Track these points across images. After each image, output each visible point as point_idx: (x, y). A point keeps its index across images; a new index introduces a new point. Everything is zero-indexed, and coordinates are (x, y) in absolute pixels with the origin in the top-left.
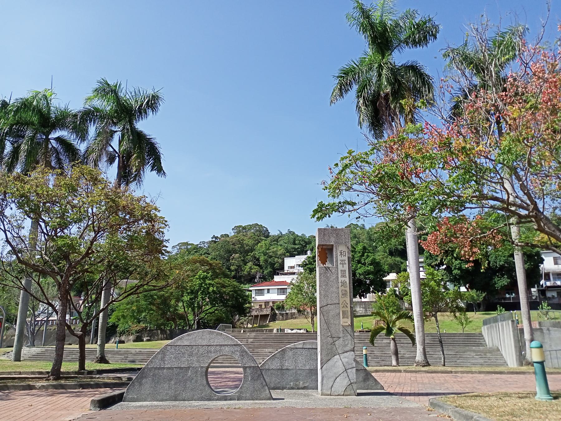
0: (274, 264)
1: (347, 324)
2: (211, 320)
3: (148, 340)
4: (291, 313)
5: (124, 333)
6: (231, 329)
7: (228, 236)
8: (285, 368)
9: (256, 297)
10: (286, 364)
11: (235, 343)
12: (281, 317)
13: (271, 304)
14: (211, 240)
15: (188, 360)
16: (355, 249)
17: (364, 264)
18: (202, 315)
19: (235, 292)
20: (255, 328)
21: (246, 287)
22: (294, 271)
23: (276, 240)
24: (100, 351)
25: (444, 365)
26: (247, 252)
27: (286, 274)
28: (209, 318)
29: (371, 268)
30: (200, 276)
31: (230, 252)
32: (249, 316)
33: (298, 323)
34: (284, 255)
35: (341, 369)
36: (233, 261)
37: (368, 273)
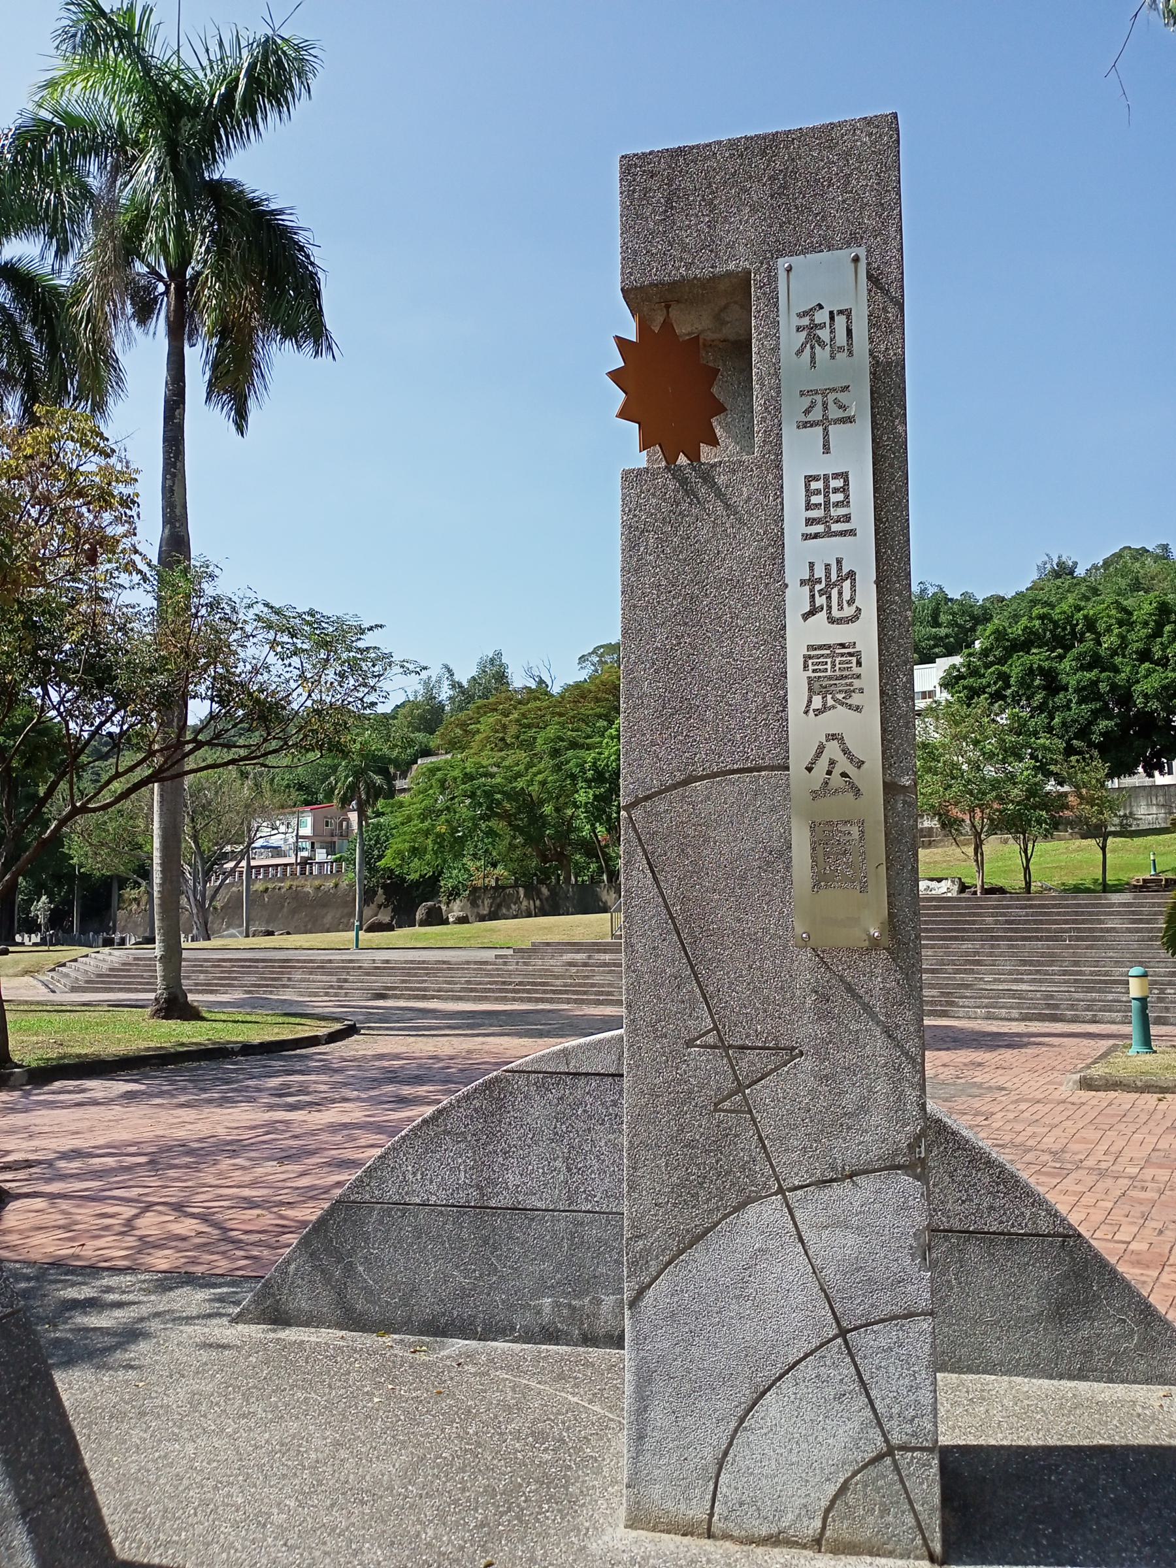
5: (458, 894)
8: (504, 1200)
16: (1130, 614)
24: (164, 978)
33: (938, 858)
35: (797, 1317)
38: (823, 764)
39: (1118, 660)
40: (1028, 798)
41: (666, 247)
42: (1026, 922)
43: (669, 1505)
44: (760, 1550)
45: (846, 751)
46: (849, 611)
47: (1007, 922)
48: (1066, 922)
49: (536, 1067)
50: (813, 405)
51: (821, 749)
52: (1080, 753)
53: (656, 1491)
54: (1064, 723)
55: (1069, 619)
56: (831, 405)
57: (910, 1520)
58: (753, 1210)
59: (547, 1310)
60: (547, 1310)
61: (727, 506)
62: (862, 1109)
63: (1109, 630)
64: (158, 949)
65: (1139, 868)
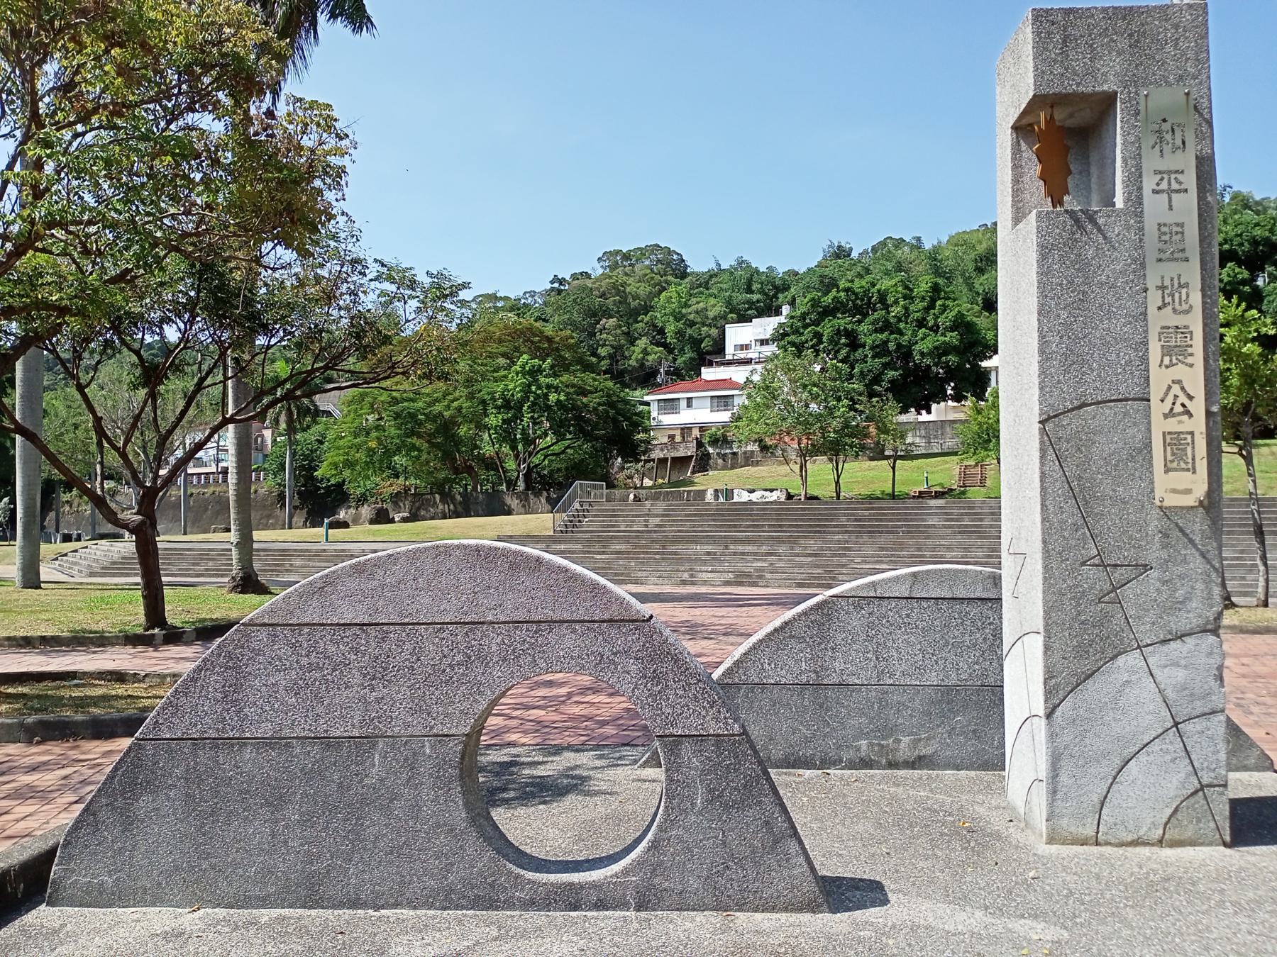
0: (701, 341)
1: (1190, 501)
2: (559, 470)
3: (404, 520)
4: (745, 453)
5: (366, 500)
6: (605, 491)
7: (588, 276)
8: (835, 679)
9: (661, 417)
10: (838, 665)
11: (613, 613)
12: (720, 461)
13: (696, 433)
14: (549, 286)
15: (363, 700)
16: (911, 290)
17: (935, 328)
18: (536, 460)
19: (611, 404)
20: (660, 486)
21: (636, 395)
22: (750, 356)
23: (705, 282)
24: (240, 560)
25: (1266, 604)
26: (634, 314)
27: (730, 363)
28: (555, 466)
29: (952, 338)
30: (523, 367)
31: (595, 314)
32: (646, 461)
33: (764, 474)
34: (724, 317)
35: (1151, 717)
36: (604, 336)
37: (944, 350)
38: (1170, 399)
39: (902, 325)
40: (843, 429)
41: (1063, 71)
42: (870, 520)
43: (1073, 829)
44: (1129, 849)
45: (1183, 388)
46: (1185, 307)
47: (856, 520)
48: (899, 520)
49: (853, 594)
50: (1162, 179)
51: (1170, 388)
52: (880, 395)
53: (1065, 821)
54: (862, 373)
55: (866, 292)
56: (1173, 182)
57: (1212, 825)
58: (1121, 660)
59: (864, 748)
60: (864, 748)
61: (1105, 238)
62: (1188, 598)
63: (896, 302)
64: (233, 536)
65: (915, 483)
